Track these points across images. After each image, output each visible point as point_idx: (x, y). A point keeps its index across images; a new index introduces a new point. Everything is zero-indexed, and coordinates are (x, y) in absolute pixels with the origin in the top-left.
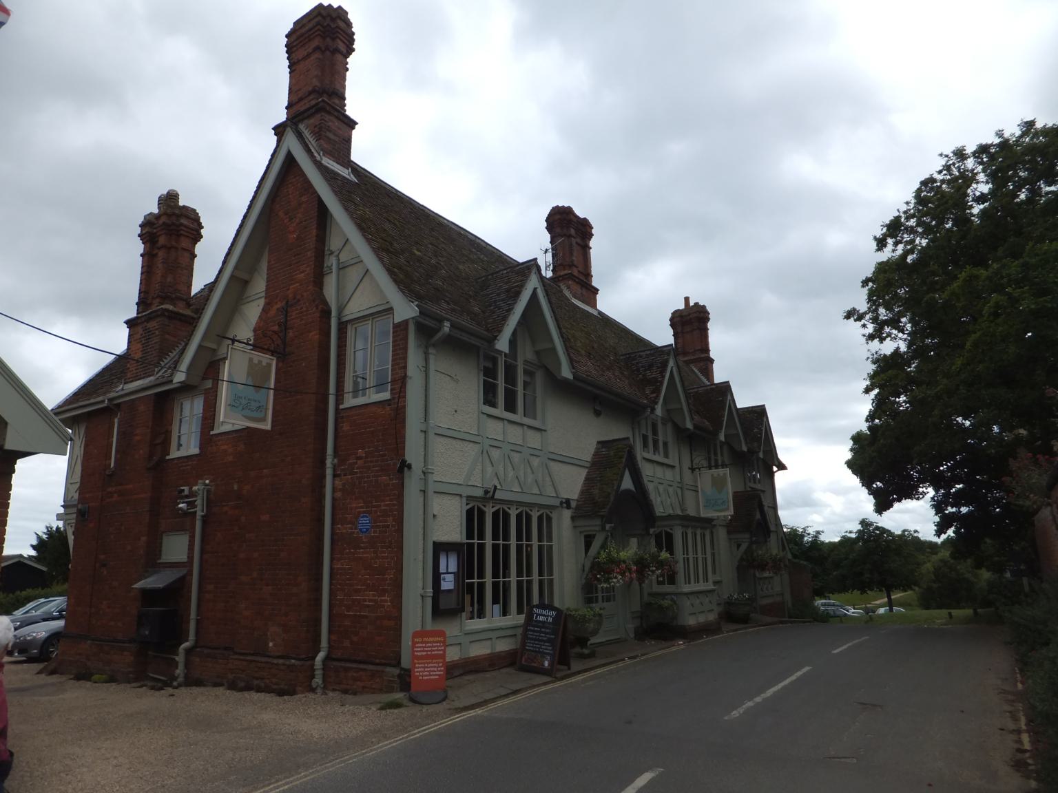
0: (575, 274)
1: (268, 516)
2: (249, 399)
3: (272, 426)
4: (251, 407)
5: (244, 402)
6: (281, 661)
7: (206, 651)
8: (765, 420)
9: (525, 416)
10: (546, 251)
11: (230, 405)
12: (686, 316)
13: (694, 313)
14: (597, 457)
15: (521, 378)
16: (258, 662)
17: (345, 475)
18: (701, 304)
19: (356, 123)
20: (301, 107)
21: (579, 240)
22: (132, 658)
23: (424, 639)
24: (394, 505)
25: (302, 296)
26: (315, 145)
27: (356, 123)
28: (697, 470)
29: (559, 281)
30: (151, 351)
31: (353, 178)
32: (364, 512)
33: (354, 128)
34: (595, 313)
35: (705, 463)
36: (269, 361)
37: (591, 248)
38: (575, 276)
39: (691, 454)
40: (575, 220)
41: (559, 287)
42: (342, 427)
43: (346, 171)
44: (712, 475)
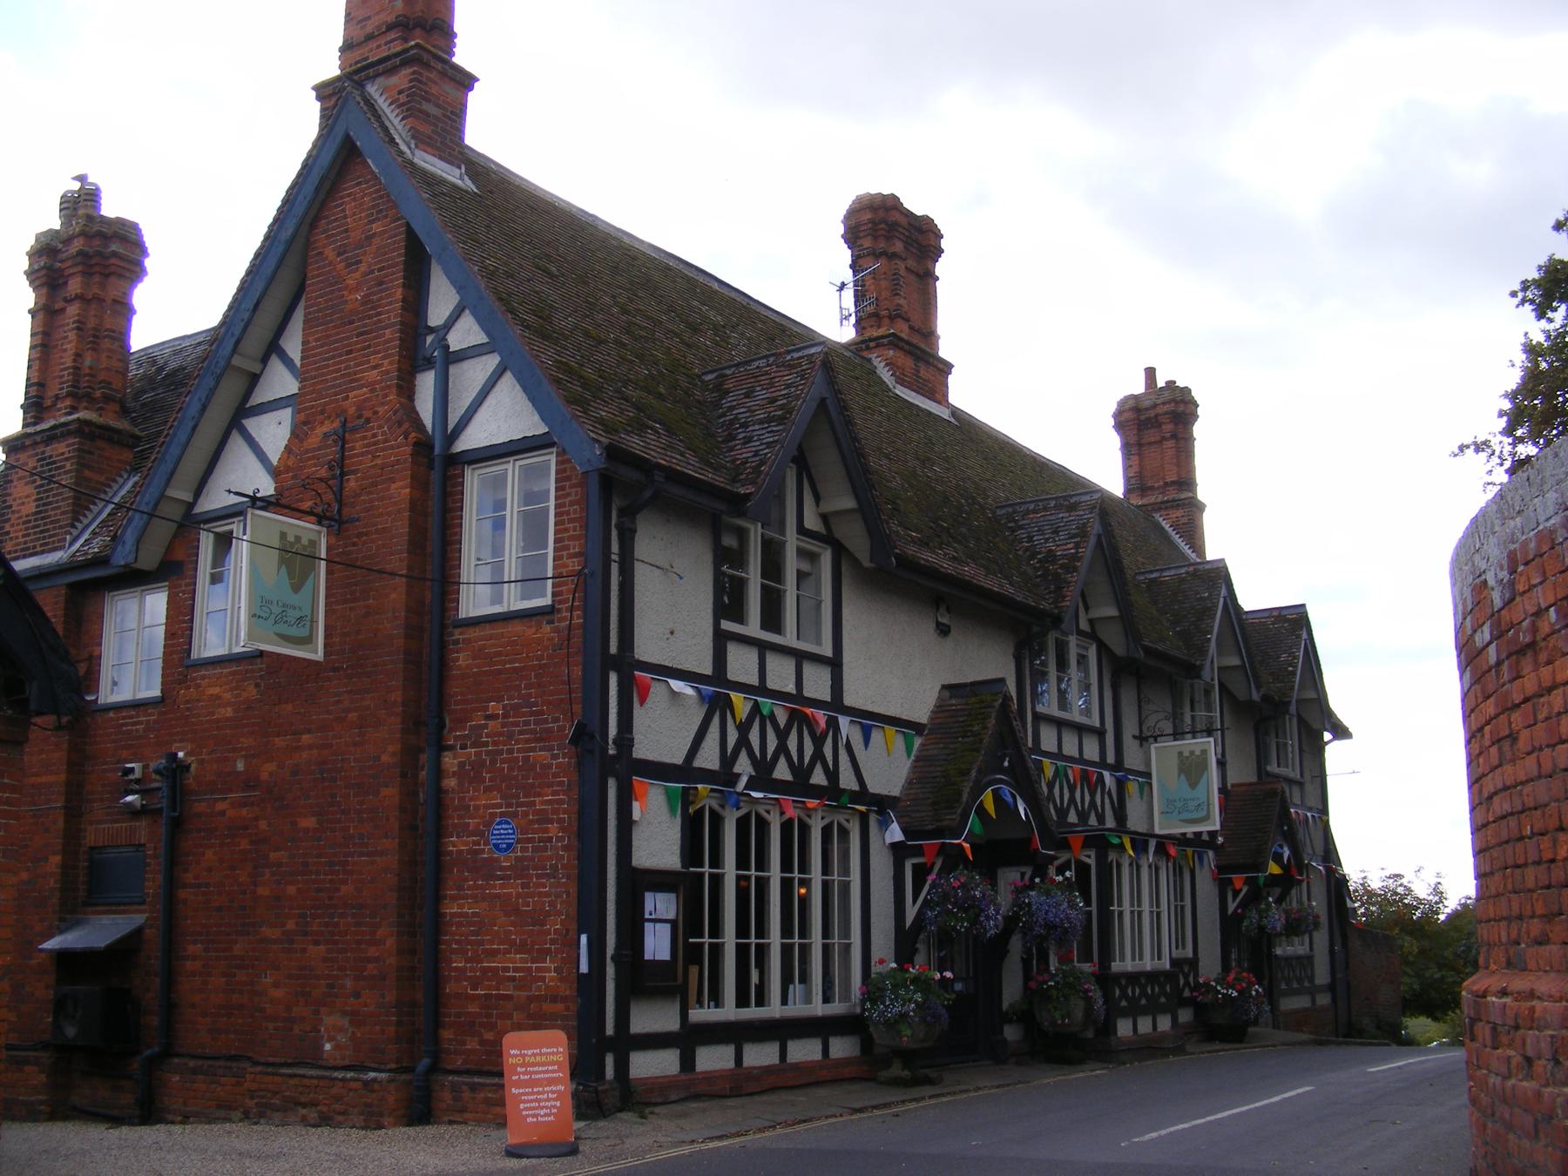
0: (903, 335)
1: (314, 819)
2: (284, 606)
3: (326, 654)
4: (289, 619)
5: (276, 610)
6: (350, 1075)
7: (192, 1063)
8: (1305, 636)
9: (798, 639)
10: (842, 286)
11: (255, 615)
12: (1147, 409)
13: (1164, 404)
14: (939, 715)
15: (792, 564)
16: (303, 1076)
17: (464, 747)
18: (1180, 384)
19: (477, 80)
20: (375, 52)
21: (911, 263)
22: (43, 1077)
23: (535, 1119)
24: (561, 802)
25: (376, 413)
26: (400, 127)
27: (477, 80)
28: (1151, 740)
29: (868, 348)
30: (57, 502)
31: (468, 184)
32: (502, 815)
33: (471, 88)
34: (945, 414)
35: (1168, 727)
36: (313, 536)
37: (938, 279)
38: (901, 339)
39: (1140, 707)
40: (903, 221)
41: (869, 360)
42: (458, 659)
43: (457, 172)
44: (1180, 754)
